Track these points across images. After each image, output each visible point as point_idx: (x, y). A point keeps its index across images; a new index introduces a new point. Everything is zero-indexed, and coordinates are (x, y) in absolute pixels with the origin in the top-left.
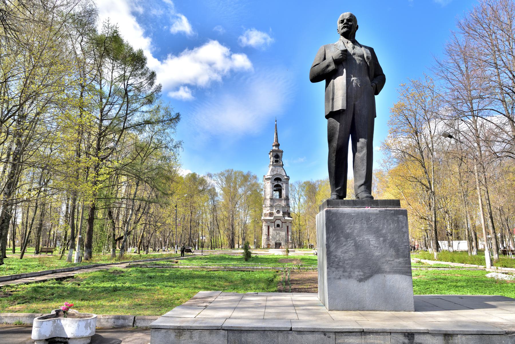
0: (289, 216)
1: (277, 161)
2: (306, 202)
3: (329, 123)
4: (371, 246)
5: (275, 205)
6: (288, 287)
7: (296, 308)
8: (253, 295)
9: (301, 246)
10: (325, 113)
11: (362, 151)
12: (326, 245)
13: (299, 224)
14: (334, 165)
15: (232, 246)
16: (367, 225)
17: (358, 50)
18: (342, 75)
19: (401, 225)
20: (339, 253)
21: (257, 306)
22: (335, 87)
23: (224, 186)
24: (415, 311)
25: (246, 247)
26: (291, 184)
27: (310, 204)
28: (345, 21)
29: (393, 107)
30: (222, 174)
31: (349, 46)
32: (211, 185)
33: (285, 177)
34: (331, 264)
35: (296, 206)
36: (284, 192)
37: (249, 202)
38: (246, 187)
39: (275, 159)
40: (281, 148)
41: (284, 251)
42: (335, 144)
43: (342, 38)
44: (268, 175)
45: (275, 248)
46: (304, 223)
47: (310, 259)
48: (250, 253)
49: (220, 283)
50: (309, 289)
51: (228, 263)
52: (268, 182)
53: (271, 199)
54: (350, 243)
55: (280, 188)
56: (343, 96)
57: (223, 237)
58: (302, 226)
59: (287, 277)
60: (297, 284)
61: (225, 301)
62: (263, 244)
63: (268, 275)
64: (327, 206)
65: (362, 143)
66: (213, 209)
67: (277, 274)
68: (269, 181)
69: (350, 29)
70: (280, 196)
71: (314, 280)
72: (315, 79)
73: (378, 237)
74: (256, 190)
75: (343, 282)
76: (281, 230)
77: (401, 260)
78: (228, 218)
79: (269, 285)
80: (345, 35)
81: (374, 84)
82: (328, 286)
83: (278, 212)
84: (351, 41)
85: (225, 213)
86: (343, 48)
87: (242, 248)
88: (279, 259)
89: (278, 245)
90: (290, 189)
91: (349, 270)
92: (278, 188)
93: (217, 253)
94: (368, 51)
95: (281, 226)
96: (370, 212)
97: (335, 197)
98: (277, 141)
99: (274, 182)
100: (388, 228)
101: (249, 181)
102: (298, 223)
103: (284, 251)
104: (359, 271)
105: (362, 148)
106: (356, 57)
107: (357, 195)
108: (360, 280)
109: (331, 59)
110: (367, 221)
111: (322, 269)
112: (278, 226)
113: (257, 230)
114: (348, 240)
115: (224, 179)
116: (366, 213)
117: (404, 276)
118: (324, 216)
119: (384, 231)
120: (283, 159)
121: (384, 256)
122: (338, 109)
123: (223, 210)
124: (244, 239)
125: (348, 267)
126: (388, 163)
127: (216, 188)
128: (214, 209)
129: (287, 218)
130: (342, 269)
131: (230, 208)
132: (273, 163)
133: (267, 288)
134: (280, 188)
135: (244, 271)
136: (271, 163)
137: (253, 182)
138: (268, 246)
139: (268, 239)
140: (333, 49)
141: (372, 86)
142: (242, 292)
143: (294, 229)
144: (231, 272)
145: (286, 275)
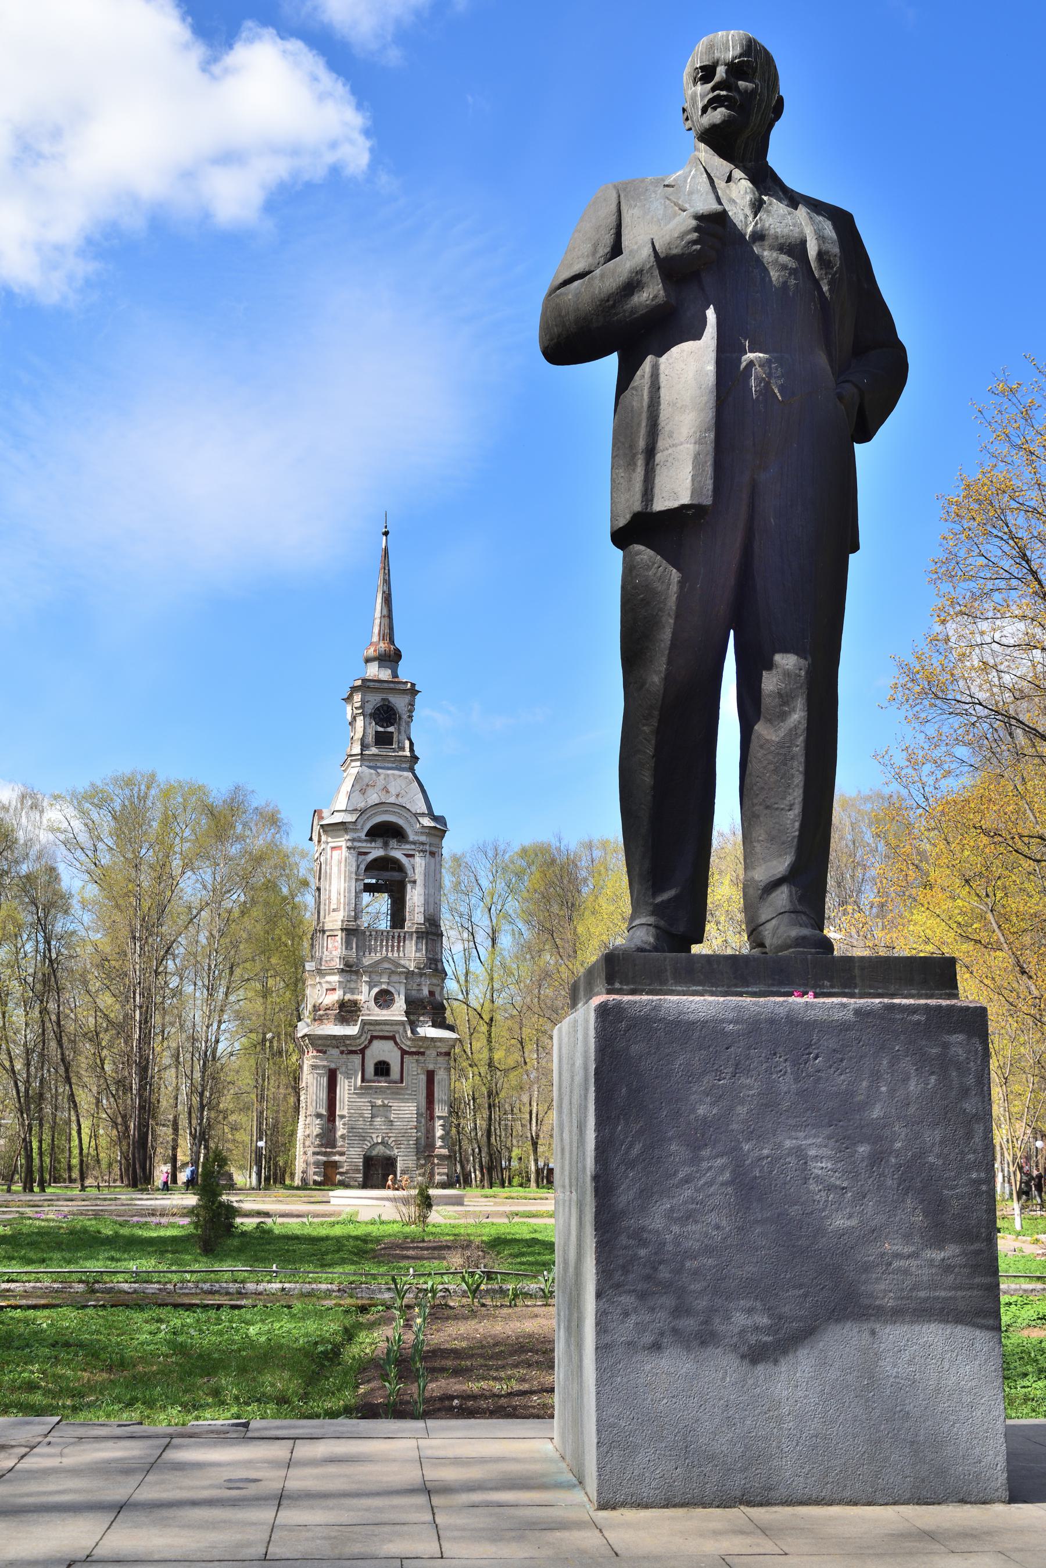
0: (440, 1023)
1: (383, 740)
2: (529, 951)
3: (630, 571)
4: (813, 1187)
5: (367, 961)
6: (414, 1388)
7: (436, 1500)
8: (220, 1437)
9: (495, 1173)
10: (613, 518)
11: (783, 716)
12: (596, 1178)
13: (491, 1064)
14: (647, 778)
15: (138, 1175)
16: (797, 1080)
17: (780, 219)
18: (698, 337)
19: (956, 1083)
20: (656, 1220)
21: (238, 1496)
22: (663, 392)
23: (105, 859)
24: (1013, 1499)
25: (210, 1181)
26: (456, 860)
27: (548, 958)
28: (721, 72)
29: (957, 494)
30: (97, 798)
31: (739, 193)
32: (33, 853)
33: (427, 822)
34: (618, 1277)
35: (475, 966)
36: (415, 898)
37: (235, 945)
38: (223, 869)
39: (374, 728)
40: (406, 672)
41: (406, 1201)
42: (655, 679)
43: (704, 153)
44: (339, 805)
45: (365, 1185)
46: (517, 1056)
47: (535, 1241)
48: (232, 1212)
49: (60, 1370)
50: (516, 1401)
51: (112, 1266)
52: (333, 842)
53: (352, 933)
54: (716, 1167)
55: (396, 875)
56: (699, 442)
57: (94, 1128)
58: (506, 1071)
59: (409, 1337)
60: (457, 1372)
61: (75, 1472)
62: (299, 1166)
63: (311, 1326)
64: (600, 985)
65: (787, 674)
66: (45, 982)
67: (363, 1319)
68: (342, 842)
69: (743, 113)
70: (398, 916)
71: (537, 1353)
72: (568, 342)
73: (845, 1142)
74: (271, 886)
75: (670, 1368)
76: (397, 1093)
77: (951, 1251)
78: (121, 1028)
79: (312, 1379)
80: (716, 138)
81: (849, 390)
82: (600, 1382)
83: (384, 999)
84: (744, 170)
85: (106, 1000)
86: (706, 204)
87: (190, 1183)
88: (378, 1240)
89: (377, 1171)
90: (447, 880)
91: (702, 1303)
92: (385, 877)
93: (56, 1208)
94: (828, 229)
95: (395, 1069)
96: (811, 1015)
97: (644, 936)
98: (389, 634)
99: (365, 846)
100: (895, 1094)
101: (240, 838)
102: (485, 1055)
103: (406, 1201)
104: (750, 1311)
105: (785, 698)
106: (768, 255)
107: (754, 931)
108: (758, 1354)
109: (646, 252)
110: (795, 1063)
111: (574, 1303)
112: (382, 1069)
113: (271, 1091)
114: (705, 1153)
115: (105, 822)
116: (793, 1021)
117: (962, 1333)
118: (592, 1033)
119: (876, 1113)
120: (416, 731)
121: (874, 1234)
122: (674, 504)
123: (95, 985)
124: (201, 1137)
125: (697, 1286)
126: (928, 768)
127: (61, 868)
128: (49, 981)
129: (428, 1031)
130: (668, 1301)
131: (134, 976)
132: (364, 746)
133: (305, 1397)
134: (396, 875)
135: (189, 1307)
136: (357, 750)
137: (259, 843)
138: (329, 1176)
139: (327, 1138)
140: (657, 204)
141: (840, 397)
142: (167, 1419)
143: (465, 1087)
144: (121, 1315)
145: (408, 1326)
